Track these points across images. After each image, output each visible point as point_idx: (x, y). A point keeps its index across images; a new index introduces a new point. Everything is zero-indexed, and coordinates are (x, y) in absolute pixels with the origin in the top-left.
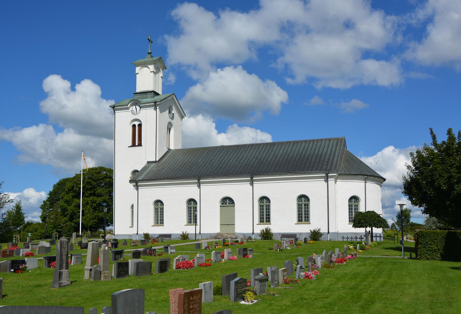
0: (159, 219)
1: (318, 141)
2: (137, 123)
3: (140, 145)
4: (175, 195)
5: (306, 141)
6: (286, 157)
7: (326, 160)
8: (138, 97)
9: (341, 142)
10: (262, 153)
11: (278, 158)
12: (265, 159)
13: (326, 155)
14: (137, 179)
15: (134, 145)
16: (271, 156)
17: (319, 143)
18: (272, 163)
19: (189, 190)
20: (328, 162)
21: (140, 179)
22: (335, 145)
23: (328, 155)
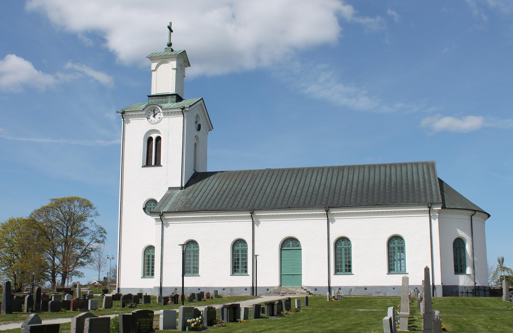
2: (154, 136)
3: (158, 163)
4: (216, 235)
6: (365, 185)
7: (422, 190)
9: (431, 166)
11: (355, 186)
12: (338, 188)
13: (419, 183)
15: (148, 164)
16: (344, 183)
18: (348, 192)
19: (238, 227)
20: (425, 192)
21: (165, 210)
22: (425, 170)
23: (421, 183)
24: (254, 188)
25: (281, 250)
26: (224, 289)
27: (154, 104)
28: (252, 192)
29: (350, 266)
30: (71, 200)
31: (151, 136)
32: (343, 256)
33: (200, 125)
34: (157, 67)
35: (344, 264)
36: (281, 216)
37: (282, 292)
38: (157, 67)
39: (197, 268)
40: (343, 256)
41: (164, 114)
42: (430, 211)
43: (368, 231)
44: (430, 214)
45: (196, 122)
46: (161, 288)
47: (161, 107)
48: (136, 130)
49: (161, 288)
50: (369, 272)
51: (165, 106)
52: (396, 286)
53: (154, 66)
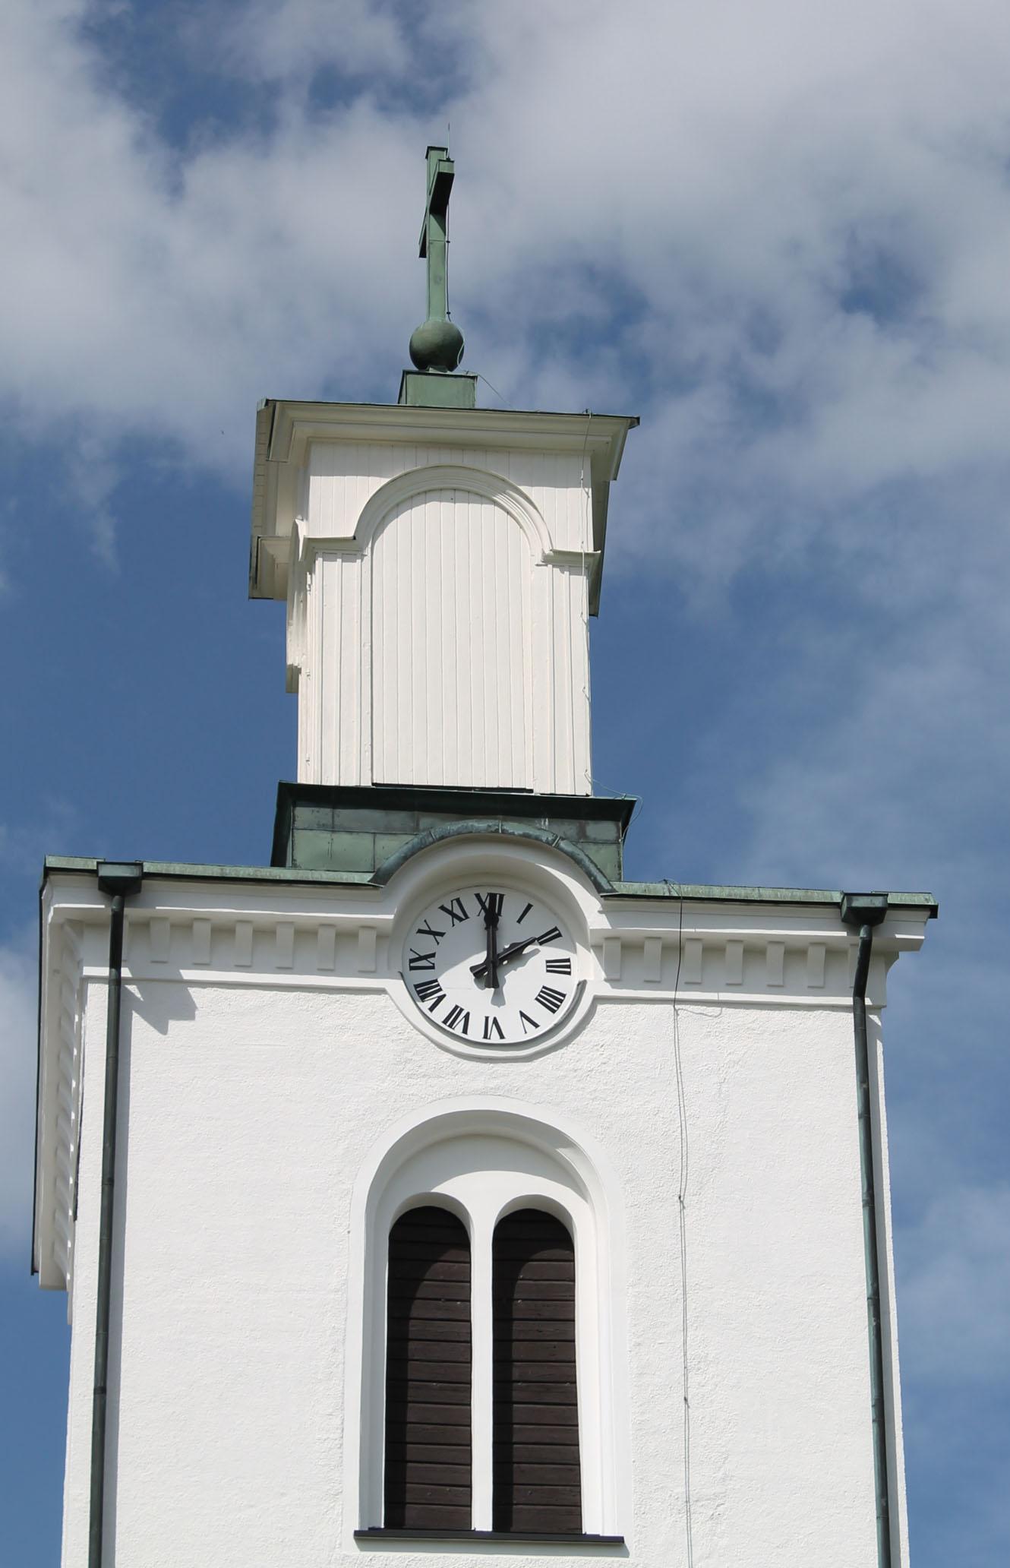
2: (483, 1197)
34: (377, 516)
38: (377, 516)
41: (622, 956)
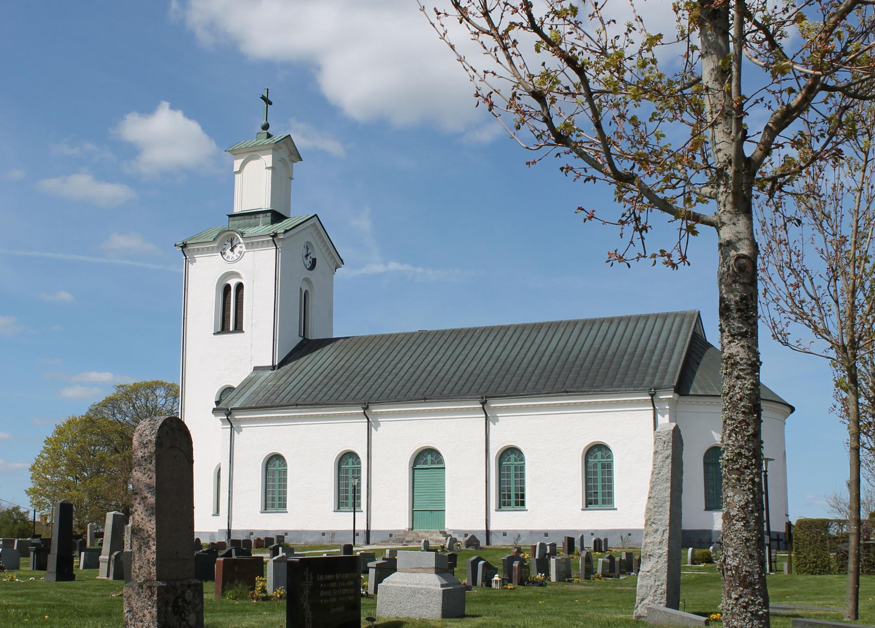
0: (274, 497)
1: (638, 318)
2: (233, 282)
3: (238, 328)
4: (312, 443)
5: (611, 320)
7: (653, 364)
8: (236, 223)
10: (509, 347)
13: (653, 352)
14: (228, 406)
15: (224, 329)
17: (640, 325)
19: (344, 432)
20: (657, 368)
24: (385, 365)
25: (414, 469)
26: (323, 534)
27: (234, 229)
28: (379, 372)
29: (523, 496)
30: (152, 387)
31: (228, 282)
32: (513, 479)
33: (314, 261)
34: (243, 166)
35: (513, 494)
36: (449, 412)
37: (407, 539)
38: (243, 166)
39: (285, 500)
40: (513, 479)
41: (247, 245)
42: (652, 400)
43: (551, 435)
44: (654, 406)
45: (307, 256)
46: (229, 532)
47: (242, 234)
48: (205, 273)
49: (229, 532)
50: (554, 508)
51: (250, 231)
52: (597, 530)
53: (237, 164)
